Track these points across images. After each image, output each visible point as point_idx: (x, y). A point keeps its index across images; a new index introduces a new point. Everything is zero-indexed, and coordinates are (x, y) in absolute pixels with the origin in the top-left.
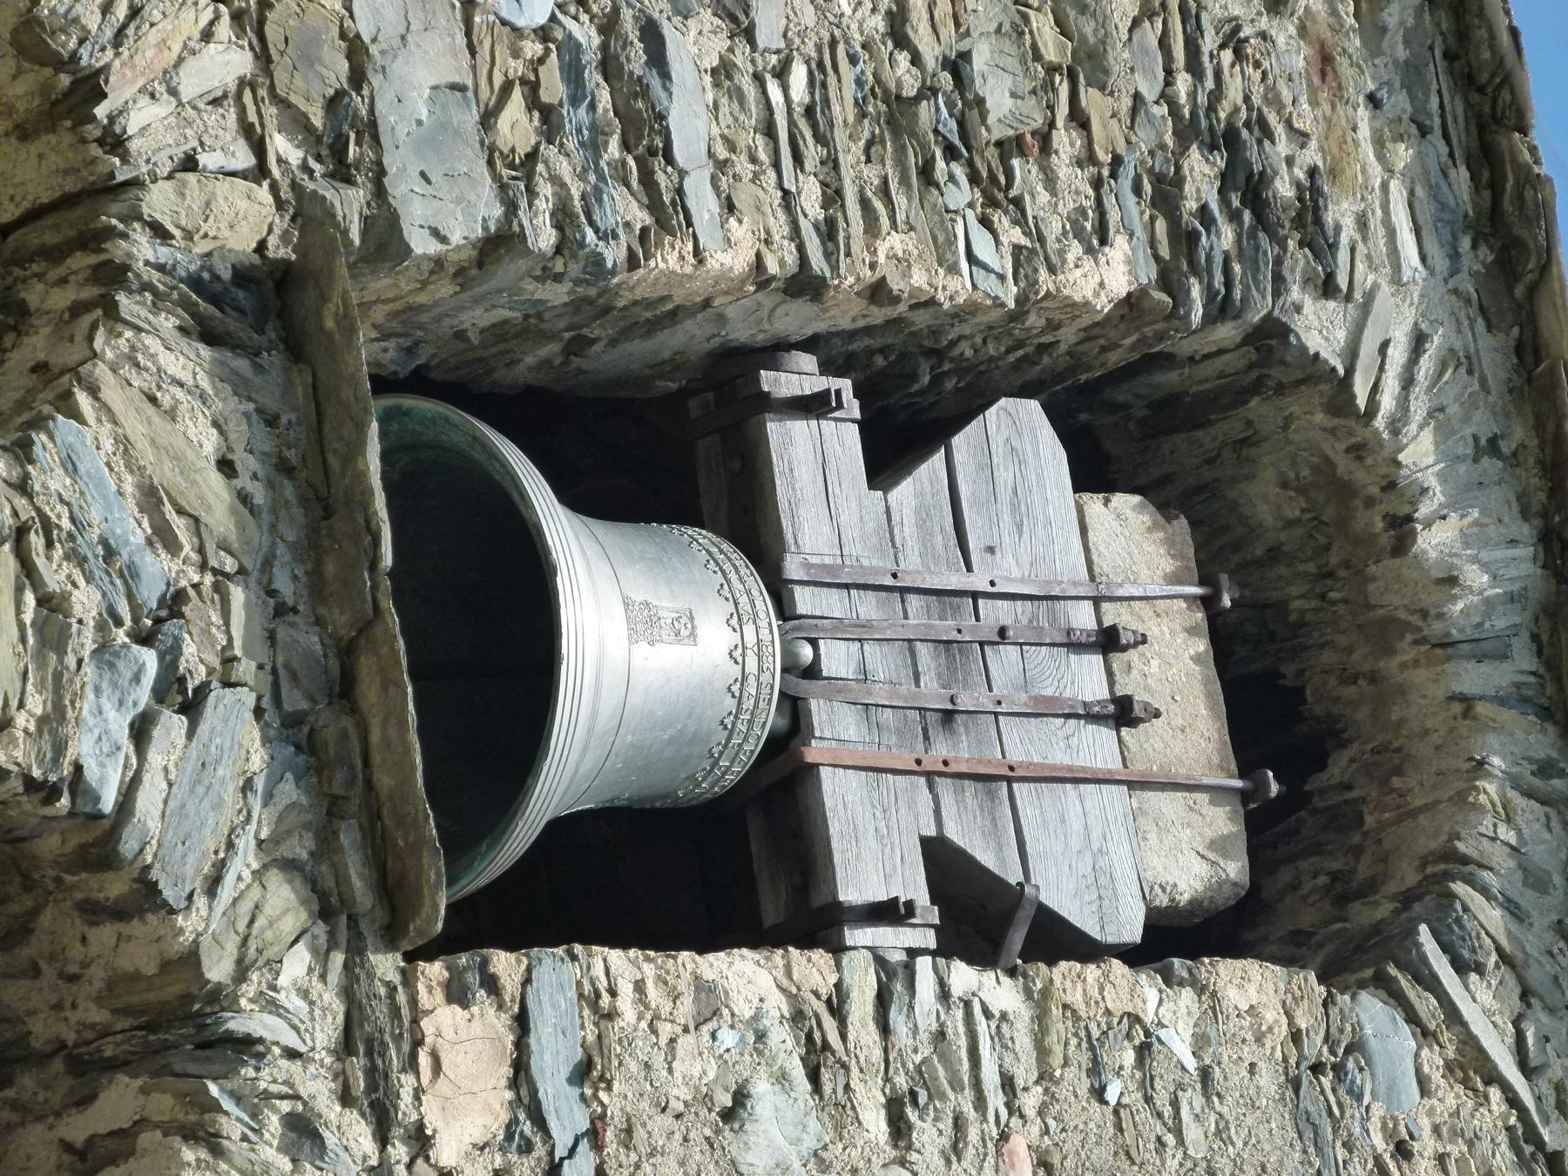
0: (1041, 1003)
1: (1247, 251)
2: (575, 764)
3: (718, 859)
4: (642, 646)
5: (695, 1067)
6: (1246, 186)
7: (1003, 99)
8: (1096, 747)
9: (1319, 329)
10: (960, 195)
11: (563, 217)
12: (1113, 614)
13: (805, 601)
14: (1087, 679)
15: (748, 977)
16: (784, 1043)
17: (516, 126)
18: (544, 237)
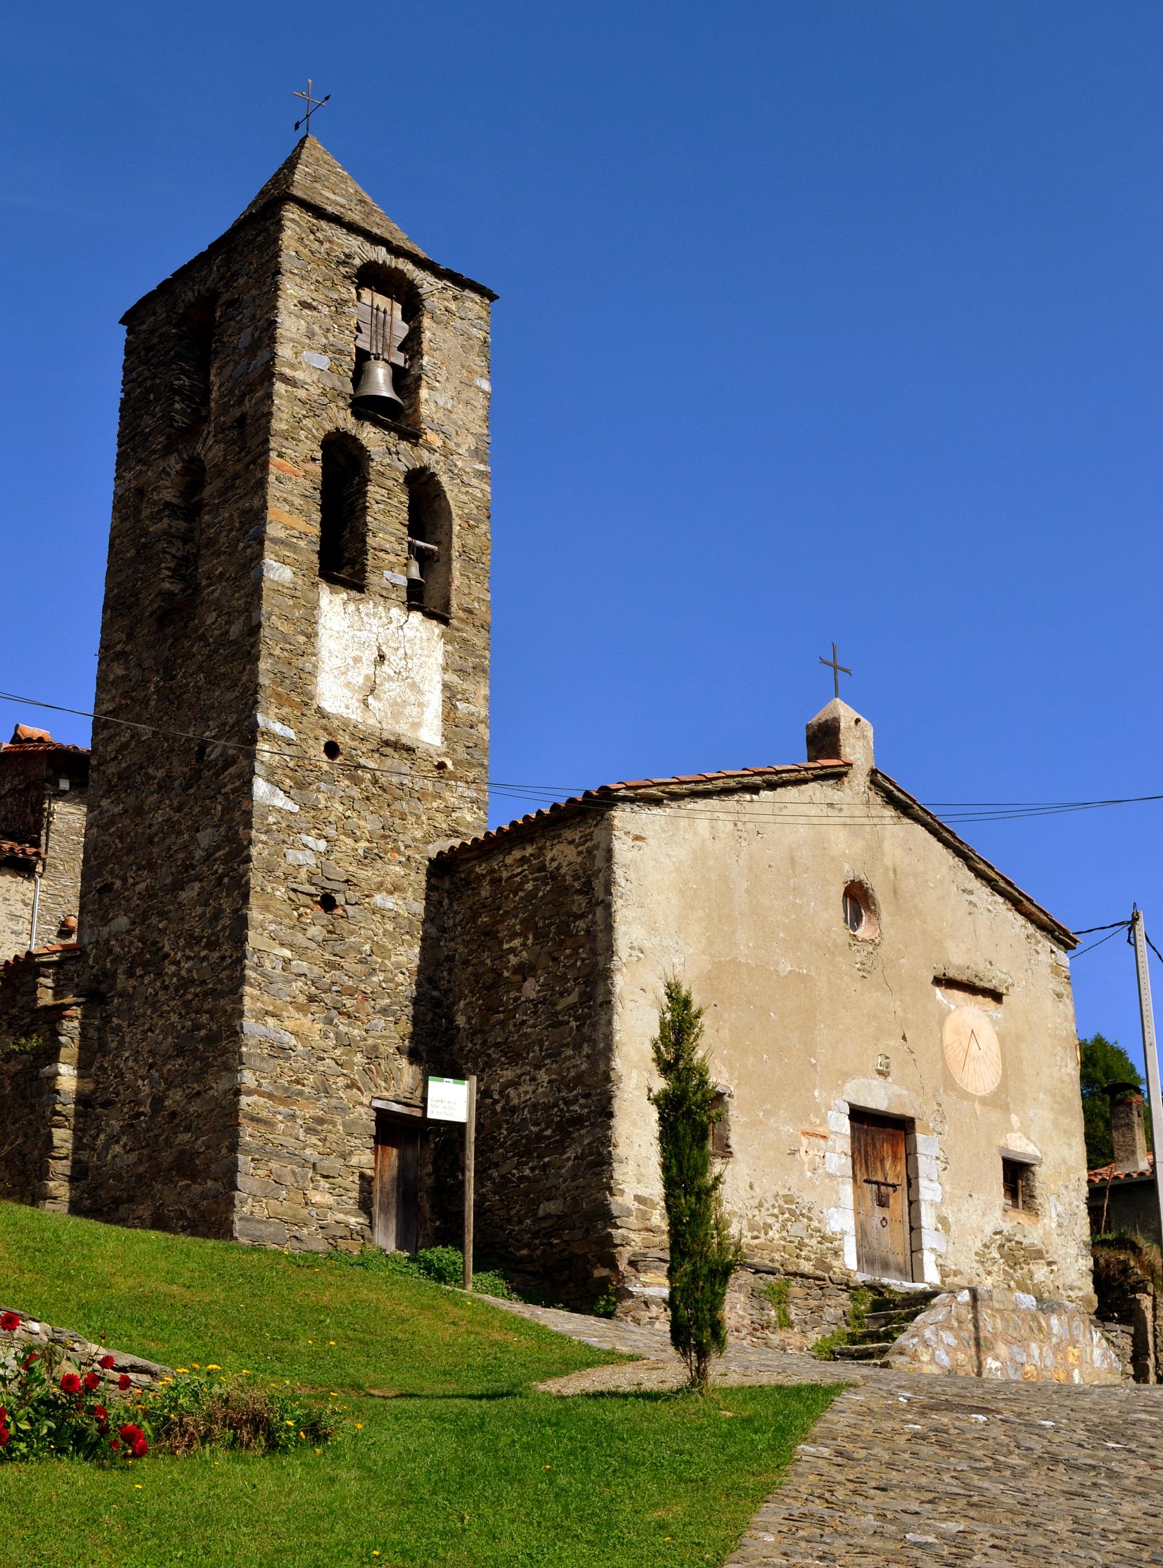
9: (357, 262)
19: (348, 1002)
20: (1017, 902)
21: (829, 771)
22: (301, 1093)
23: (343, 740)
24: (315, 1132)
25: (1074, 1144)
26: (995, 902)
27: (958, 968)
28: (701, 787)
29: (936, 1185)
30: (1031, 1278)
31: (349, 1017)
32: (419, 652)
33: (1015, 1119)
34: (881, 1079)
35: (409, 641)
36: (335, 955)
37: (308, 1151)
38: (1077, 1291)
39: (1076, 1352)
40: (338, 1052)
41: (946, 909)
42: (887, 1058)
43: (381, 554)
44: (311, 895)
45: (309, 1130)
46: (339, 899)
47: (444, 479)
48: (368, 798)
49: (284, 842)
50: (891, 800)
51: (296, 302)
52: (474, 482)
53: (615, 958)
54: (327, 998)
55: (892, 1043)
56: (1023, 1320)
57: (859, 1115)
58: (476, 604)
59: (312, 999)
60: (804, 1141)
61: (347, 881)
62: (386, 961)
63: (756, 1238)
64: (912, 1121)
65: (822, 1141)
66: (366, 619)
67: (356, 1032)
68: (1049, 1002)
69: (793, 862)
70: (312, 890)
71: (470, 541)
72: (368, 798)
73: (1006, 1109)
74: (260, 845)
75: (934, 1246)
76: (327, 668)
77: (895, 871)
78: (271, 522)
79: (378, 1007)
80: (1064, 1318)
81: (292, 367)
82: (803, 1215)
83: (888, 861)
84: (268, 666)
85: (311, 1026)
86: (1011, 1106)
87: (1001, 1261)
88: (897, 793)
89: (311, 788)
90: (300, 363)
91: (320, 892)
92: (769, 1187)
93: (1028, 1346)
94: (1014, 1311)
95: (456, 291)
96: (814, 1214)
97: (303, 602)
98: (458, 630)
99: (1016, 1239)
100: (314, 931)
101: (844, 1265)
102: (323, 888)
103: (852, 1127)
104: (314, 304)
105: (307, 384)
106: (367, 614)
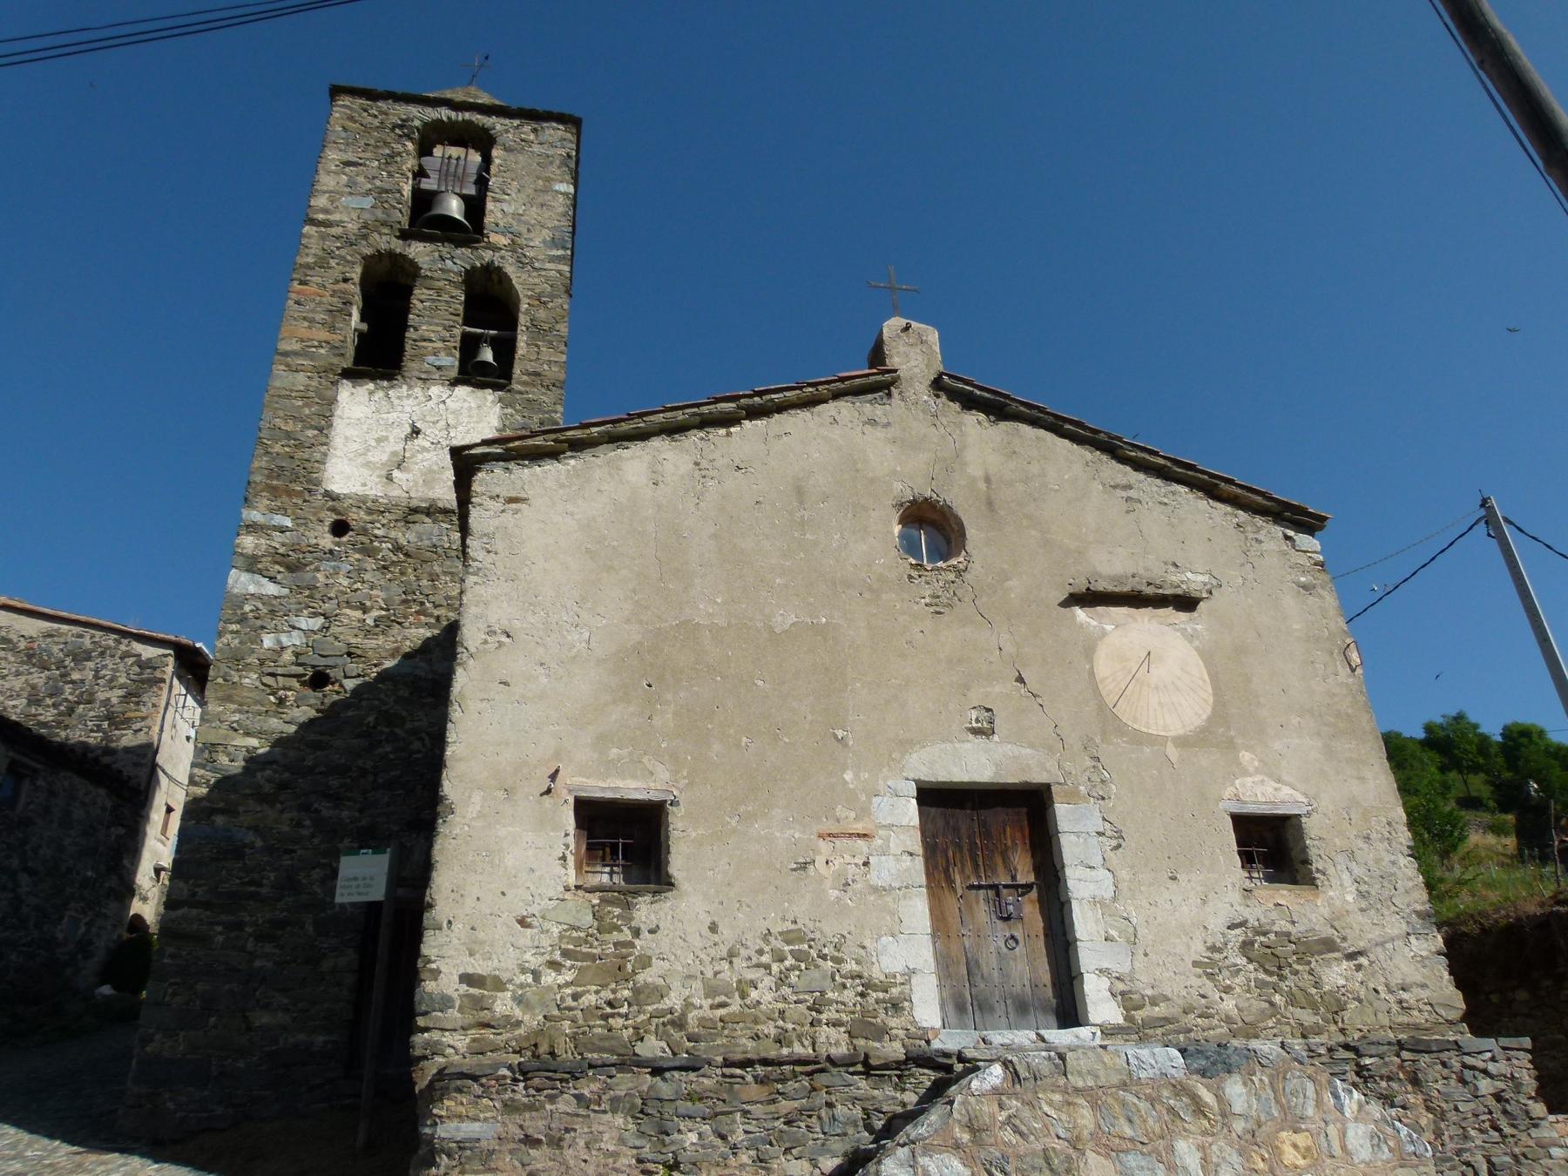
3: (475, 207)
5: (499, 215)
19: (334, 782)
20: (1211, 488)
22: (254, 896)
23: (356, 517)
25: (1369, 775)
26: (1174, 493)
27: (1112, 579)
28: (625, 427)
29: (1102, 873)
30: (1317, 985)
33: (1245, 756)
34: (980, 741)
38: (1415, 990)
39: (1302, 1140)
41: (1056, 501)
42: (988, 710)
47: (510, 269)
49: (263, 627)
50: (969, 402)
52: (548, 266)
53: (460, 649)
55: (997, 689)
56: (1152, 1100)
57: (932, 796)
60: (824, 846)
63: (723, 1005)
64: (1048, 786)
65: (860, 842)
66: (396, 402)
68: (1290, 602)
69: (800, 492)
70: (300, 670)
71: (542, 314)
72: (384, 567)
73: (1230, 746)
74: (229, 636)
75: (1105, 965)
76: (338, 453)
80: (1262, 1078)
81: (326, 211)
82: (824, 957)
83: (975, 470)
84: (263, 464)
86: (1239, 741)
87: (1251, 967)
92: (750, 924)
93: (1171, 1149)
94: (1124, 1086)
96: (850, 950)
99: (1276, 928)
101: (914, 1022)
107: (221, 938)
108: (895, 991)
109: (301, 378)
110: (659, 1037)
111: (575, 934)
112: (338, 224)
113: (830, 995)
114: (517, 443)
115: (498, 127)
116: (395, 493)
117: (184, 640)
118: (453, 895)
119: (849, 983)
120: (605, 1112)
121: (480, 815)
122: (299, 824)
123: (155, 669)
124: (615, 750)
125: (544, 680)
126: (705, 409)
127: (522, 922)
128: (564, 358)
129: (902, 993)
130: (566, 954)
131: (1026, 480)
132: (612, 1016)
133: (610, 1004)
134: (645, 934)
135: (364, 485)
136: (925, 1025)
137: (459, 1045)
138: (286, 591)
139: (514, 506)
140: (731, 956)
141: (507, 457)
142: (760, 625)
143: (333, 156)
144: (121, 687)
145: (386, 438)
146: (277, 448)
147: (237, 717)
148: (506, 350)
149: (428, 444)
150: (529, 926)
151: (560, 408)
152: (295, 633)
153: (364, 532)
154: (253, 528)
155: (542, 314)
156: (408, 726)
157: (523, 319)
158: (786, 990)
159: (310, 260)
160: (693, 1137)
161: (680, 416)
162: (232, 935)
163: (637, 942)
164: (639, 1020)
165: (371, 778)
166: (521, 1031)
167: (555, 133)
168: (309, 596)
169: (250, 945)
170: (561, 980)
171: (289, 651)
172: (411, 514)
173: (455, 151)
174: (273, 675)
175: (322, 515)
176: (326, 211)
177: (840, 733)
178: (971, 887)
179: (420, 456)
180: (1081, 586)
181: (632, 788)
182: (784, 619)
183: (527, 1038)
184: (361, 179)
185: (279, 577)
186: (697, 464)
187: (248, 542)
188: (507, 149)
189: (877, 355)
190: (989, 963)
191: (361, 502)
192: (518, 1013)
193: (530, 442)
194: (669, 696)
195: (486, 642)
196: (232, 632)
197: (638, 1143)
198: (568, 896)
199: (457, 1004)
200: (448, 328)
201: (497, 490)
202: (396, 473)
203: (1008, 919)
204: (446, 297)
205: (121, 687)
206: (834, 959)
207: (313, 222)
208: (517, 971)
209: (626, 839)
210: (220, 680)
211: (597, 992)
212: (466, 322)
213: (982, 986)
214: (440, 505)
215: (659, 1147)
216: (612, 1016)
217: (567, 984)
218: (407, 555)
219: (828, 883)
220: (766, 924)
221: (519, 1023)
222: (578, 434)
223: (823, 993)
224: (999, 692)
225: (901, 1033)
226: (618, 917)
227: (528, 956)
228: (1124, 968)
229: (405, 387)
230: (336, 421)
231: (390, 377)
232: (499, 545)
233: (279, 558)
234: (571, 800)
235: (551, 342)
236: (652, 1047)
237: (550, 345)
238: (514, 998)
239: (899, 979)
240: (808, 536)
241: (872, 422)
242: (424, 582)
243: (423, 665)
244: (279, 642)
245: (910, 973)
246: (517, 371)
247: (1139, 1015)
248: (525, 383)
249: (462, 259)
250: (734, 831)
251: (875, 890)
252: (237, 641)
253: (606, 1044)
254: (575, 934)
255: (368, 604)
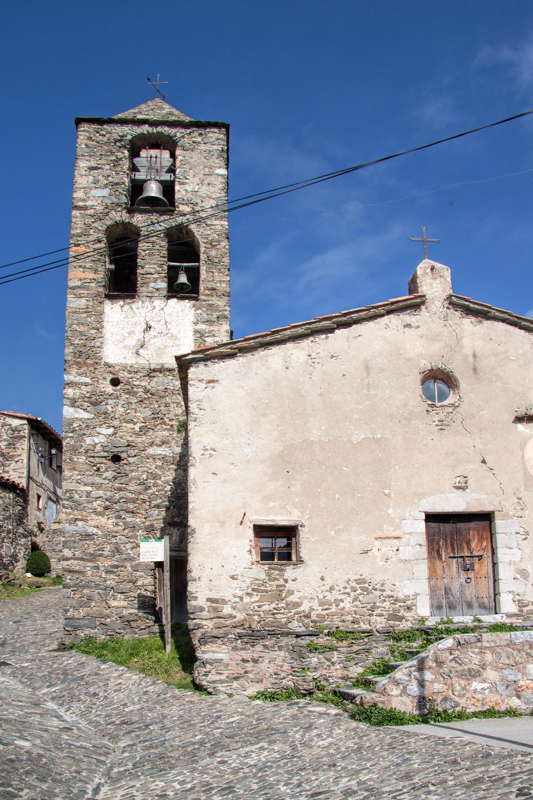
0: (179, 167)
1: (124, 142)
2: (160, 196)
3: (168, 188)
4: (153, 190)
5: (184, 193)
6: (120, 141)
7: (113, 158)
8: (158, 160)
9: (129, 137)
10: (121, 162)
11: (124, 191)
12: (149, 156)
13: (149, 178)
14: (154, 159)
15: (177, 187)
16: (182, 186)
17: (117, 193)
18: (125, 193)
19: (131, 506)
21: (400, 304)
22: (101, 555)
23: (123, 375)
24: (112, 572)
28: (268, 339)
29: (516, 550)
31: (133, 513)
32: (176, 318)
34: (460, 491)
35: (167, 315)
36: (122, 484)
37: (108, 582)
40: (126, 531)
43: (148, 276)
44: (105, 457)
45: (107, 572)
46: (123, 456)
48: (141, 401)
49: (84, 434)
50: (468, 311)
51: (86, 169)
53: (190, 458)
54: (117, 507)
55: (471, 467)
58: (218, 285)
59: (106, 508)
60: (377, 543)
61: (129, 445)
62: (158, 481)
64: (493, 513)
66: (136, 311)
67: (138, 520)
69: (367, 368)
70: (106, 454)
71: (213, 253)
72: (141, 401)
75: (512, 589)
77: (474, 356)
78: (70, 280)
79: (153, 505)
81: (84, 200)
82: (376, 589)
84: (71, 350)
85: (108, 522)
88: (472, 305)
89: (102, 404)
90: (89, 197)
91: (111, 455)
92: (340, 576)
95: (201, 131)
96: (387, 587)
97: (94, 313)
98: (205, 301)
100: (106, 474)
102: (112, 452)
103: (427, 526)
104: (99, 166)
105: (94, 206)
106: (137, 308)
107: (90, 572)
108: (408, 603)
109: (83, 301)
110: (299, 621)
111: (257, 582)
112: (92, 207)
113: (378, 604)
114: (210, 352)
115: (178, 135)
116: (142, 361)
117: (31, 416)
118: (200, 567)
119: (387, 599)
120: (276, 651)
121: (210, 534)
122: (117, 525)
123: (20, 431)
124: (272, 503)
125: (234, 471)
126: (313, 326)
127: (233, 578)
128: (228, 278)
129: (412, 603)
130: (254, 590)
131: (496, 355)
132: (277, 613)
133: (275, 609)
134: (290, 582)
135: (125, 358)
136: (421, 615)
137: (210, 625)
138: (93, 415)
139: (211, 384)
140: (332, 589)
141: (206, 359)
142: (345, 439)
143: (82, 164)
144: (5, 440)
145: (134, 332)
146: (77, 341)
147: (79, 477)
148: (194, 276)
149: (156, 334)
150: (236, 579)
151: (228, 308)
152: (101, 436)
153: (128, 383)
154: (71, 384)
155: (213, 253)
156: (163, 479)
157: (203, 257)
158: (357, 603)
159: (79, 231)
160: (315, 659)
161: (300, 330)
162: (95, 571)
163: (287, 585)
164: (289, 615)
165: (148, 504)
166: (236, 620)
167: (215, 136)
168: (106, 417)
169: (104, 575)
170: (252, 600)
171: (99, 445)
172: (152, 372)
173: (153, 152)
174: (93, 457)
175: (105, 375)
176: (84, 200)
177: (387, 491)
178: (450, 557)
179: (153, 341)
180: (522, 412)
181: (282, 519)
182: (358, 436)
183: (239, 622)
184: (100, 177)
185: (88, 409)
186: (309, 356)
187: (70, 392)
188: (184, 149)
189: (413, 285)
190: (456, 588)
191: (124, 368)
192: (234, 613)
193: (217, 350)
194: (298, 477)
195: (203, 454)
196: (70, 437)
197: (291, 661)
198: (253, 566)
199: (207, 609)
200: (161, 266)
201: (202, 377)
202: (141, 351)
203: (468, 570)
204: (157, 247)
205: (5, 440)
206: (380, 590)
207: (77, 208)
208: (232, 597)
209: (278, 542)
210: (68, 460)
211: (269, 605)
212: (169, 260)
213: (452, 598)
214: (166, 366)
215: (300, 663)
216: (277, 613)
217: (255, 602)
218: (152, 394)
219: (378, 559)
220: (348, 576)
221: (235, 617)
222: (244, 344)
223: (375, 603)
224: (472, 468)
225: (411, 619)
226: (278, 574)
227: (237, 591)
228: (520, 590)
229: (140, 302)
230: (105, 324)
231: (133, 297)
232: (204, 405)
233: (86, 399)
234: (252, 526)
235: (220, 269)
236: (296, 626)
237: (220, 271)
238: (232, 607)
239: (411, 597)
240: (372, 392)
241: (408, 326)
242: (162, 408)
243: (167, 449)
244: (94, 441)
245: (416, 595)
246: (202, 288)
247: (525, 609)
248: (208, 295)
249: (165, 222)
250: (332, 538)
251: (401, 561)
252: (73, 441)
253: (275, 624)
254: (257, 582)
255: (135, 420)
